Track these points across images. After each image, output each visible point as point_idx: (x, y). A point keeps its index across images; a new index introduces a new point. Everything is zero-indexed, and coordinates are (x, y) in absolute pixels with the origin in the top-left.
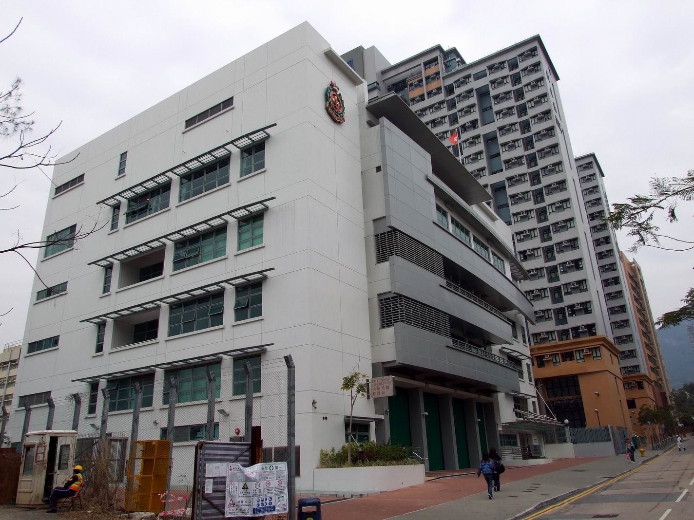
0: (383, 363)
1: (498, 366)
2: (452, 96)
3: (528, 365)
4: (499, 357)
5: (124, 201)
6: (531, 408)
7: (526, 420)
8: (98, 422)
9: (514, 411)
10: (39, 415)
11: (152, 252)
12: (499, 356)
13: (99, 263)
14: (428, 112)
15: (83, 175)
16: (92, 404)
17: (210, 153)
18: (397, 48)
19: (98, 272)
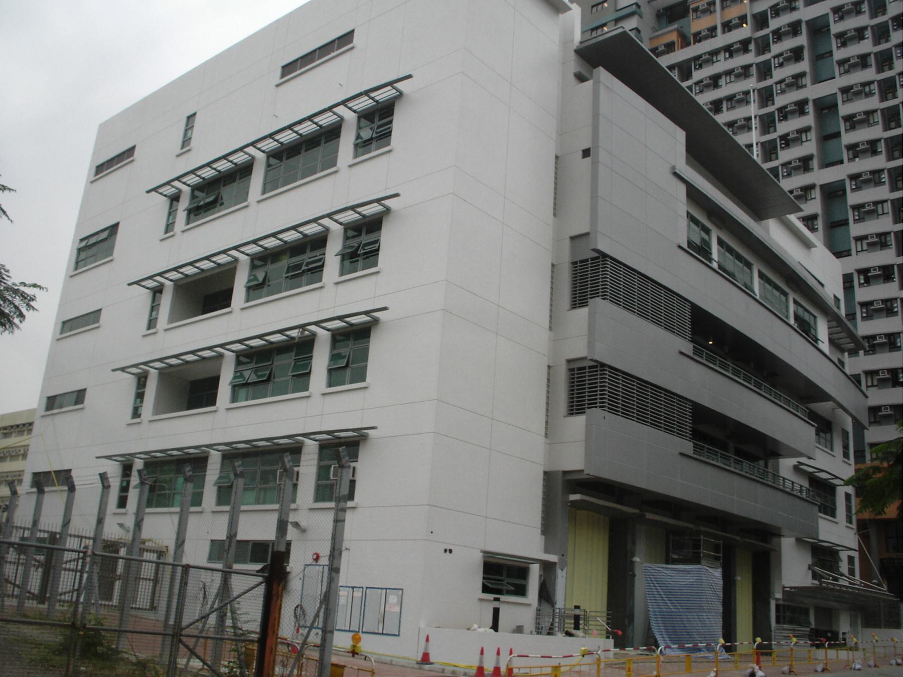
0: (565, 473)
1: (779, 493)
2: (765, 32)
3: (848, 496)
4: (793, 483)
5: (186, 190)
6: (844, 567)
7: (824, 585)
8: (130, 522)
9: (809, 568)
10: (54, 500)
11: (217, 271)
13: (143, 283)
14: (721, 56)
15: (134, 148)
16: (199, 490)
17: (310, 118)
19: (143, 296)
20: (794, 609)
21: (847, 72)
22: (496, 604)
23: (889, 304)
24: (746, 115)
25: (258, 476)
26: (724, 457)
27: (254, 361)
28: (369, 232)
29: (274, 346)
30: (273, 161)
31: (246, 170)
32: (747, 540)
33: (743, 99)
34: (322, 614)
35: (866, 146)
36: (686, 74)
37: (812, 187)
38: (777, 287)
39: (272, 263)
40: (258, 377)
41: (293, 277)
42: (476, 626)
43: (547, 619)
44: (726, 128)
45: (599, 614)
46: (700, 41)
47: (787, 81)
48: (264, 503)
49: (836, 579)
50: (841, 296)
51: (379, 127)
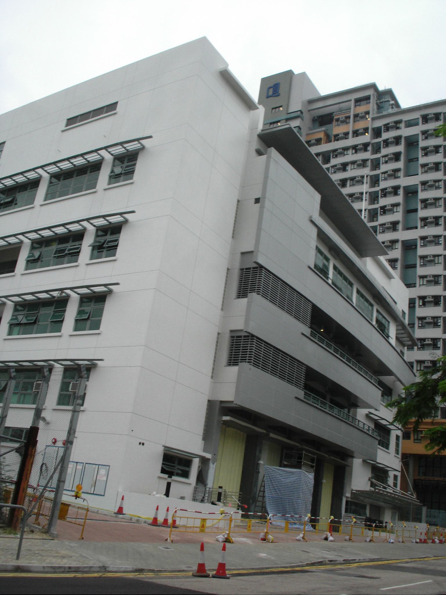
0: (222, 402)
1: (356, 430)
3: (398, 437)
4: (364, 424)
7: (377, 490)
9: (369, 480)
11: (8, 248)
12: (365, 422)
14: (350, 152)
18: (331, 77)
20: (356, 506)
21: (426, 172)
22: (169, 480)
23: (435, 320)
24: (361, 191)
25: (21, 386)
26: (322, 403)
27: (26, 310)
28: (112, 234)
29: (41, 300)
30: (54, 180)
31: (35, 184)
32: (332, 458)
33: (360, 181)
34: (59, 467)
35: (432, 220)
36: (327, 160)
37: (396, 241)
38: (367, 300)
39: (45, 247)
40: (28, 320)
41: (58, 257)
42: (154, 493)
43: (200, 494)
44: (347, 198)
45: (234, 494)
46: (338, 140)
47: (389, 173)
48: (23, 403)
49: (385, 488)
50: (407, 311)
51: (127, 167)
